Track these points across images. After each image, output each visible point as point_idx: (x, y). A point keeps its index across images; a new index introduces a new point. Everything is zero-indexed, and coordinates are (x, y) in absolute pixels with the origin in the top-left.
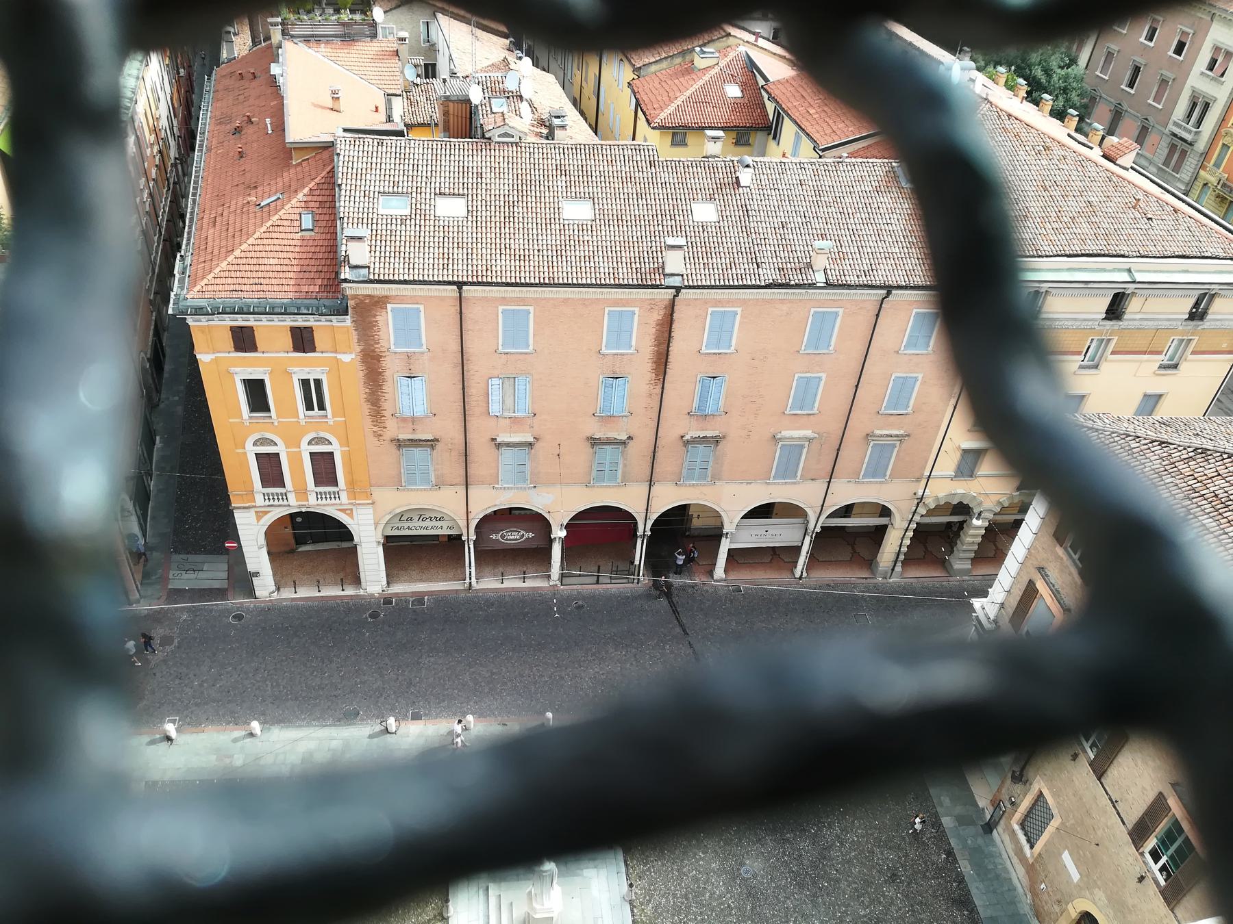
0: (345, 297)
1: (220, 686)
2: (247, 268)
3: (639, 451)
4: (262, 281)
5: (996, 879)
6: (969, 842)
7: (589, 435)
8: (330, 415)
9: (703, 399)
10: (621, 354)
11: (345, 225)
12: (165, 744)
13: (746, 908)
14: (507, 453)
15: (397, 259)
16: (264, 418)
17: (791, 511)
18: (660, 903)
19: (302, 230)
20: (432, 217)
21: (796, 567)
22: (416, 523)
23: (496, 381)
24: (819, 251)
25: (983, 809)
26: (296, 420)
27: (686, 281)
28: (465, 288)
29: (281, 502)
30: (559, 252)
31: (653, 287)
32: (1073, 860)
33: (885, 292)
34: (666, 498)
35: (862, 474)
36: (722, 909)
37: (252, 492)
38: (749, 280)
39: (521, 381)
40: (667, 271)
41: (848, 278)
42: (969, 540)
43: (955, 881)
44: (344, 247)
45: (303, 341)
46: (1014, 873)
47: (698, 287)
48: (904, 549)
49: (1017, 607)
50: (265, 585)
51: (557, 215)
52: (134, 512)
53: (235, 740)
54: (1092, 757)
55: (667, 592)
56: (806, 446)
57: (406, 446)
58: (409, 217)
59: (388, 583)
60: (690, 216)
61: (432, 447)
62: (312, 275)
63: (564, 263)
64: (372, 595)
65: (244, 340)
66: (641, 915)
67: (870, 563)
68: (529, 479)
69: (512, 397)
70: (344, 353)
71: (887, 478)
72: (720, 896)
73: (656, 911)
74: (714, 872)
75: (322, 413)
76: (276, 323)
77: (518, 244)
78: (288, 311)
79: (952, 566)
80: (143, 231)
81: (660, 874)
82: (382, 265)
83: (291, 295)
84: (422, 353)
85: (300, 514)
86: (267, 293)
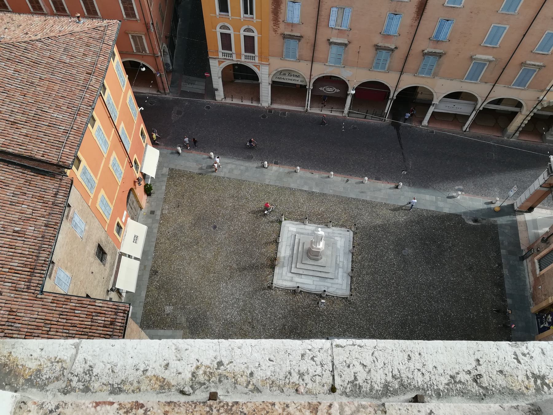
3: (399, 55)
6: (511, 262)
7: (376, 43)
8: (255, 18)
9: (439, 32)
12: (176, 155)
14: (334, 48)
16: (226, 15)
17: (470, 97)
18: (365, 256)
23: (334, 9)
26: (214, 15)
29: (229, 58)
34: (408, 81)
37: (217, 51)
39: (347, 10)
46: (528, 279)
48: (523, 125)
50: (220, 95)
52: (168, 53)
55: (397, 126)
56: (488, 64)
61: (299, 40)
66: (356, 259)
67: (503, 129)
69: (341, 19)
72: (391, 259)
75: (251, 16)
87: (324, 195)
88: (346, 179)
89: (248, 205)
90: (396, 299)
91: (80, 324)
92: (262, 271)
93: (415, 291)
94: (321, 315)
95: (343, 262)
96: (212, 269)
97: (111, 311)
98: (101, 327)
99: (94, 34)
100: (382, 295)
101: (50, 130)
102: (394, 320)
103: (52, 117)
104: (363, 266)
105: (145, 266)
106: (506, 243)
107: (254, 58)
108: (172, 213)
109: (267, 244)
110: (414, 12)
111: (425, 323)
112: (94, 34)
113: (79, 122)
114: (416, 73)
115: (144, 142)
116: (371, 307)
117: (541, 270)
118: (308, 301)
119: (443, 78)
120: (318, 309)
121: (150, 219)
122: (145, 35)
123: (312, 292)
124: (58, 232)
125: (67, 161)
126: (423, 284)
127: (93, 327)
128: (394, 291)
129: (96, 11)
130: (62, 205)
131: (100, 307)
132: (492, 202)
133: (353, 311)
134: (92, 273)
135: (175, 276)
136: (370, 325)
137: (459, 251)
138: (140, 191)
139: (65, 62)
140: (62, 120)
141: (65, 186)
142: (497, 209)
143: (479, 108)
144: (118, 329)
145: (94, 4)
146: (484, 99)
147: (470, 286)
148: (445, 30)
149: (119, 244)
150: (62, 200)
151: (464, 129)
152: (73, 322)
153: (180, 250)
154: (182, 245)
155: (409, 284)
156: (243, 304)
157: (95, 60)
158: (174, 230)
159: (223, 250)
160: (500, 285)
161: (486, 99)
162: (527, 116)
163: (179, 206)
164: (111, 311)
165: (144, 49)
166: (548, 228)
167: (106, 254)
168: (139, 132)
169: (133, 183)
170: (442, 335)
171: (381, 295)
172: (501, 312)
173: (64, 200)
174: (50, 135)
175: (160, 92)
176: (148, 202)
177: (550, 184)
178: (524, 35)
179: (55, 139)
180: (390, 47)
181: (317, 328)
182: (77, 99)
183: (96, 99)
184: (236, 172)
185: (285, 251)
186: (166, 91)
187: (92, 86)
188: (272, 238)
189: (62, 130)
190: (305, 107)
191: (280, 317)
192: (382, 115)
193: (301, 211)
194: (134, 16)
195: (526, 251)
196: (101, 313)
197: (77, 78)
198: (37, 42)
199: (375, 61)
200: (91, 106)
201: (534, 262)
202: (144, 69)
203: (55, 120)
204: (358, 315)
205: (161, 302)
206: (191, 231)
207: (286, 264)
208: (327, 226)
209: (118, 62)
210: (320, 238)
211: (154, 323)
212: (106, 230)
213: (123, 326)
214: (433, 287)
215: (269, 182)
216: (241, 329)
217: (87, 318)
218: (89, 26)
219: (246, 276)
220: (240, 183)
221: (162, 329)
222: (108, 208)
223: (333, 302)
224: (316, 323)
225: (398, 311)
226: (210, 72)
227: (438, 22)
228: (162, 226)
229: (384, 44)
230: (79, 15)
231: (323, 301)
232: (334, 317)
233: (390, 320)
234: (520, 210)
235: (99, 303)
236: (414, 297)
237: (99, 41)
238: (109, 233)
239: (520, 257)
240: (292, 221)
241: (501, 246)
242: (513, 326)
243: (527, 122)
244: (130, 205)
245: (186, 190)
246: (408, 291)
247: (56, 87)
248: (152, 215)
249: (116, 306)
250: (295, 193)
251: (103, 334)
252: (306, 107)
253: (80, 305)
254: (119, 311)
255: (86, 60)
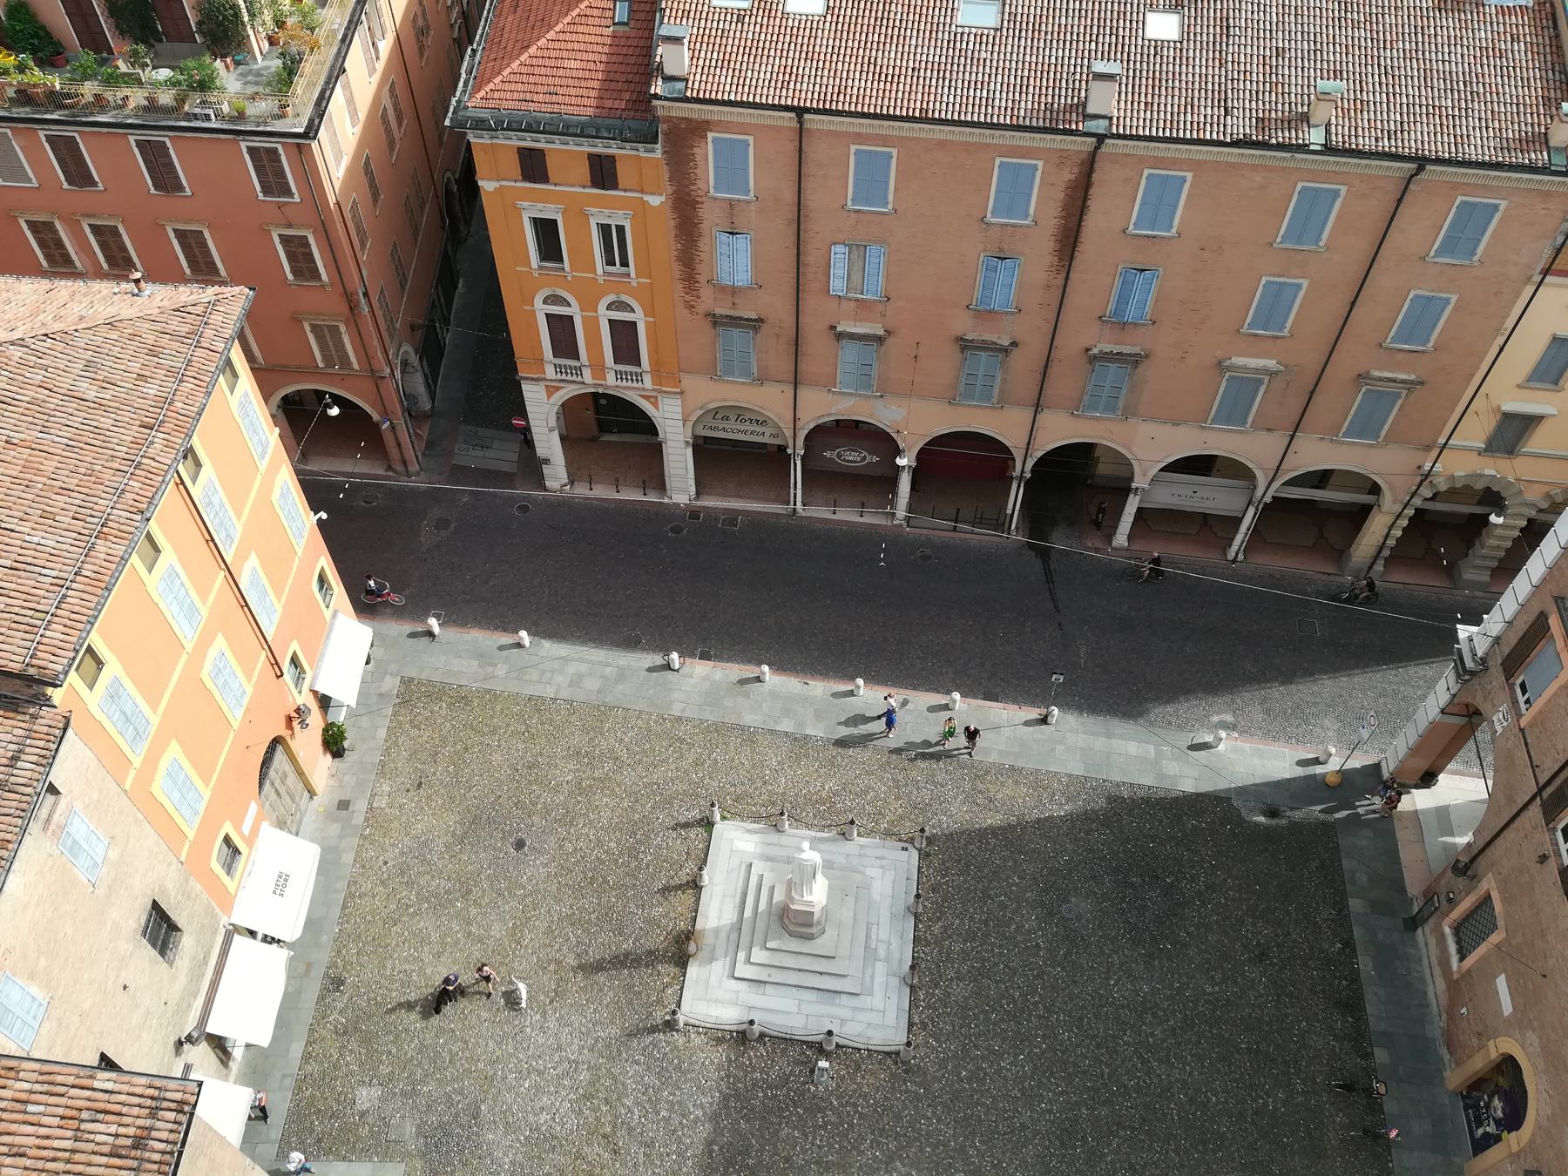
0: (656, 119)
1: (494, 585)
2: (543, 71)
3: (1024, 363)
4: (559, 90)
5: (1407, 990)
6: (1380, 936)
7: (959, 334)
8: (633, 274)
9: (1123, 300)
10: (1013, 226)
11: (666, 19)
12: (425, 640)
13: (1059, 952)
14: (850, 351)
15: (724, 70)
16: (556, 269)
17: (1237, 471)
19: (614, 24)
20: (779, 14)
21: (1230, 546)
22: (732, 424)
23: (840, 249)
24: (1321, 97)
25: (1412, 899)
26: (592, 275)
29: (635, 384)
31: (1065, 132)
32: (1509, 987)
33: (1414, 166)
34: (1058, 431)
37: (541, 361)
38: (1208, 133)
39: (873, 250)
40: (1090, 110)
41: (1361, 140)
42: (1493, 542)
44: (660, 51)
45: (603, 173)
46: (1432, 986)
47: (1131, 137)
48: (1391, 542)
50: (556, 474)
51: (948, 20)
52: (419, 368)
53: (501, 648)
55: (1044, 554)
56: (1266, 381)
57: (724, 324)
58: (748, 12)
59: (698, 494)
60: (1140, 31)
61: (756, 330)
63: (946, 90)
66: (925, 932)
67: (1340, 554)
68: (875, 384)
69: (861, 273)
70: (651, 194)
71: (1248, 426)
72: (1029, 932)
73: (945, 931)
77: (889, 57)
79: (1461, 575)
80: (463, 13)
81: (960, 890)
82: (704, 77)
83: (590, 111)
84: (749, 202)
85: (605, 395)
86: (569, 107)
89: (618, 778)
90: (1043, 1053)
91: (39, 1147)
92: (651, 974)
93: (1101, 1026)
95: (889, 943)
97: (139, 1106)
98: (102, 1155)
99: (174, 324)
100: (1003, 1042)
101: (14, 579)
102: (1038, 1120)
103: (25, 544)
104: (948, 954)
105: (309, 966)
106: (1362, 878)
107: (639, 378)
109: (666, 890)
111: (1133, 1129)
113: (102, 556)
114: (1075, 408)
115: (328, 607)
116: (969, 1080)
117: (1462, 959)
118: (781, 1066)
119: (1152, 419)
120: (813, 1089)
121: (335, 825)
122: (347, 323)
123: (796, 1037)
124: (7, 868)
125: (51, 666)
126: (1123, 1007)
127: (77, 1157)
128: (1037, 1029)
129: (213, 263)
130: (28, 790)
131: (106, 1091)
132: (1317, 758)
133: (916, 1093)
134: (125, 987)
135: (394, 994)
136: (966, 1138)
137: (1226, 904)
138: (307, 743)
139: (84, 397)
140: (53, 551)
141: (43, 736)
142: (1332, 780)
143: (1263, 497)
144: (155, 1162)
146: (1272, 473)
147: (1262, 1010)
148: (1136, 297)
149: (227, 901)
150: (29, 774)
152: (18, 1140)
155: (1081, 1008)
157: (169, 390)
160: (1352, 1004)
161: (1276, 473)
163: (420, 785)
164: (139, 1106)
165: (345, 362)
166: (1470, 834)
167: (180, 930)
168: (313, 575)
170: (1183, 1166)
171: (999, 1043)
173: (36, 776)
174: (13, 594)
175: (395, 471)
177: (1467, 706)
178: (1353, 304)
179: (25, 604)
182: (103, 495)
183: (160, 493)
184: (592, 684)
185: (721, 911)
186: (410, 468)
187: (153, 459)
188: (683, 876)
189: (49, 580)
190: (788, 503)
192: (1000, 523)
193: (771, 793)
194: (315, 275)
195: (1421, 903)
198: (10, 347)
199: (963, 380)
200: (142, 512)
202: (335, 411)
203: (32, 552)
204: (929, 1106)
205: (347, 1076)
206: (451, 857)
207: (720, 951)
208: (844, 834)
210: (810, 870)
211: (319, 1141)
213: (172, 1153)
214: (1154, 1015)
215: (683, 710)
216: (579, 1156)
217: (62, 1127)
218: (165, 303)
219: (601, 990)
220: (597, 715)
222: (191, 794)
223: (858, 1068)
224: (806, 1136)
226: (523, 413)
227: (1118, 275)
228: (367, 843)
230: (138, 275)
231: (823, 1064)
232: (860, 1114)
233: (1025, 1119)
235: (104, 1081)
237: (185, 340)
238: (195, 866)
240: (743, 821)
241: (1349, 887)
242: (1393, 1134)
243: (1401, 533)
244: (272, 784)
245: (444, 740)
246: (1078, 1029)
247: (50, 465)
249: (155, 1088)
250: (754, 739)
252: (792, 503)
253: (46, 1087)
254: (165, 1104)
255: (145, 390)
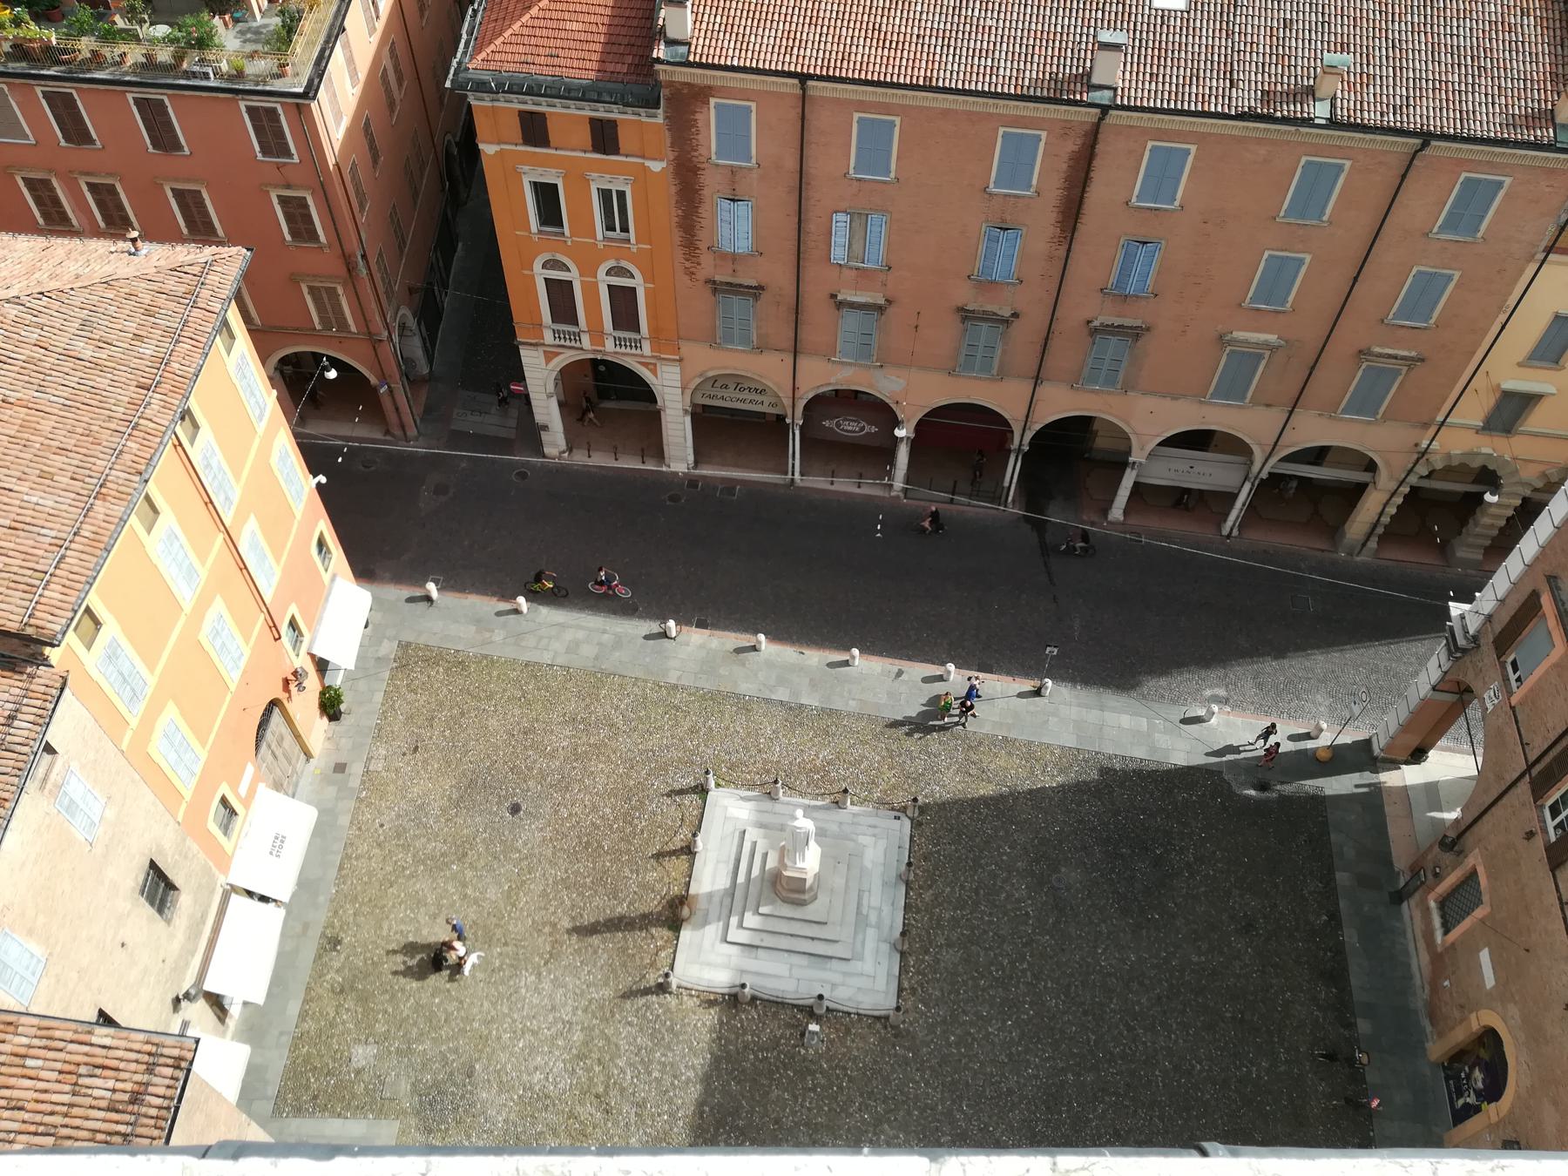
0: (658, 85)
2: (544, 33)
3: (1025, 335)
4: (561, 53)
6: (1366, 909)
7: (960, 305)
8: (633, 240)
9: (1125, 272)
14: (851, 320)
16: (556, 234)
17: (1235, 446)
18: (943, 891)
22: (730, 393)
23: (841, 217)
25: (1399, 873)
26: (593, 241)
27: (1119, 98)
28: (810, 83)
30: (946, 40)
33: (1418, 141)
34: (1057, 404)
35: (1342, 406)
36: (1016, 915)
38: (1213, 106)
39: (875, 219)
40: (1095, 80)
41: (1366, 114)
43: (1330, 951)
45: (604, 138)
48: (1386, 520)
49: (1508, 624)
50: (555, 440)
52: (417, 332)
54: (1553, 839)
55: (1040, 527)
61: (756, 297)
62: (622, 49)
64: (676, 474)
65: (534, 130)
67: (1334, 531)
69: (862, 242)
72: (1019, 901)
73: (936, 899)
74: (1017, 871)
75: (624, 235)
76: (573, 111)
78: (587, 96)
84: (750, 169)
86: (564, 69)
87: (831, 713)
88: (896, 669)
89: (613, 744)
91: (37, 1101)
94: (813, 1073)
95: (880, 910)
96: (499, 932)
97: (137, 1061)
98: (99, 1109)
99: (171, 284)
102: (1025, 1085)
103: (23, 504)
105: (306, 926)
108: (397, 770)
110: (1053, 222)
112: (172, 282)
114: (1075, 382)
115: (326, 570)
116: (957, 1044)
117: (1446, 932)
118: (772, 1029)
120: (803, 1052)
123: (787, 1001)
126: (1110, 975)
127: (75, 1111)
130: (25, 749)
131: (104, 1047)
132: (1309, 733)
133: (905, 1057)
134: (123, 945)
136: (954, 1102)
138: (304, 705)
139: (80, 356)
141: (39, 696)
142: (1323, 755)
144: (152, 1118)
145: (205, 207)
146: (1269, 449)
148: (1138, 268)
149: (223, 861)
150: (26, 733)
151: (1226, 531)
152: (16, 1094)
153: (412, 876)
154: (417, 861)
156: (581, 1038)
158: (397, 819)
159: (535, 877)
160: (1336, 975)
161: (1273, 449)
162: (1393, 495)
163: (416, 749)
164: (137, 1061)
165: (343, 325)
166: (1459, 809)
167: (177, 889)
169: (280, 684)
170: (1167, 1132)
171: (987, 1008)
172: (1338, 1057)
173: (33, 735)
175: (393, 436)
176: (329, 739)
178: (1355, 279)
180: (1000, 313)
181: (796, 1112)
183: (158, 455)
186: (408, 433)
191: (689, 1079)
192: (997, 496)
193: (765, 762)
194: (313, 236)
196: (104, 1067)
197: (109, 400)
198: (6, 305)
200: (141, 474)
201: (1428, 909)
202: (332, 374)
203: (31, 512)
208: (837, 803)
209: (243, 357)
211: (315, 1097)
212: (180, 820)
213: (168, 1108)
215: (679, 678)
216: (571, 1115)
217: (60, 1082)
218: (162, 263)
219: (595, 952)
221: (339, 1115)
223: (848, 1031)
225: (1037, 1056)
228: (363, 806)
229: (981, 306)
230: (135, 234)
232: (850, 1077)
234: (1389, 756)
235: (102, 1036)
236: (1085, 1013)
239: (1390, 893)
240: (737, 788)
242: (1375, 1103)
245: (441, 704)
247: (47, 425)
248: (339, 776)
249: (153, 1044)
251: (104, 1132)
252: (790, 473)
253: (44, 1042)
254: (162, 1060)
255: (141, 350)
